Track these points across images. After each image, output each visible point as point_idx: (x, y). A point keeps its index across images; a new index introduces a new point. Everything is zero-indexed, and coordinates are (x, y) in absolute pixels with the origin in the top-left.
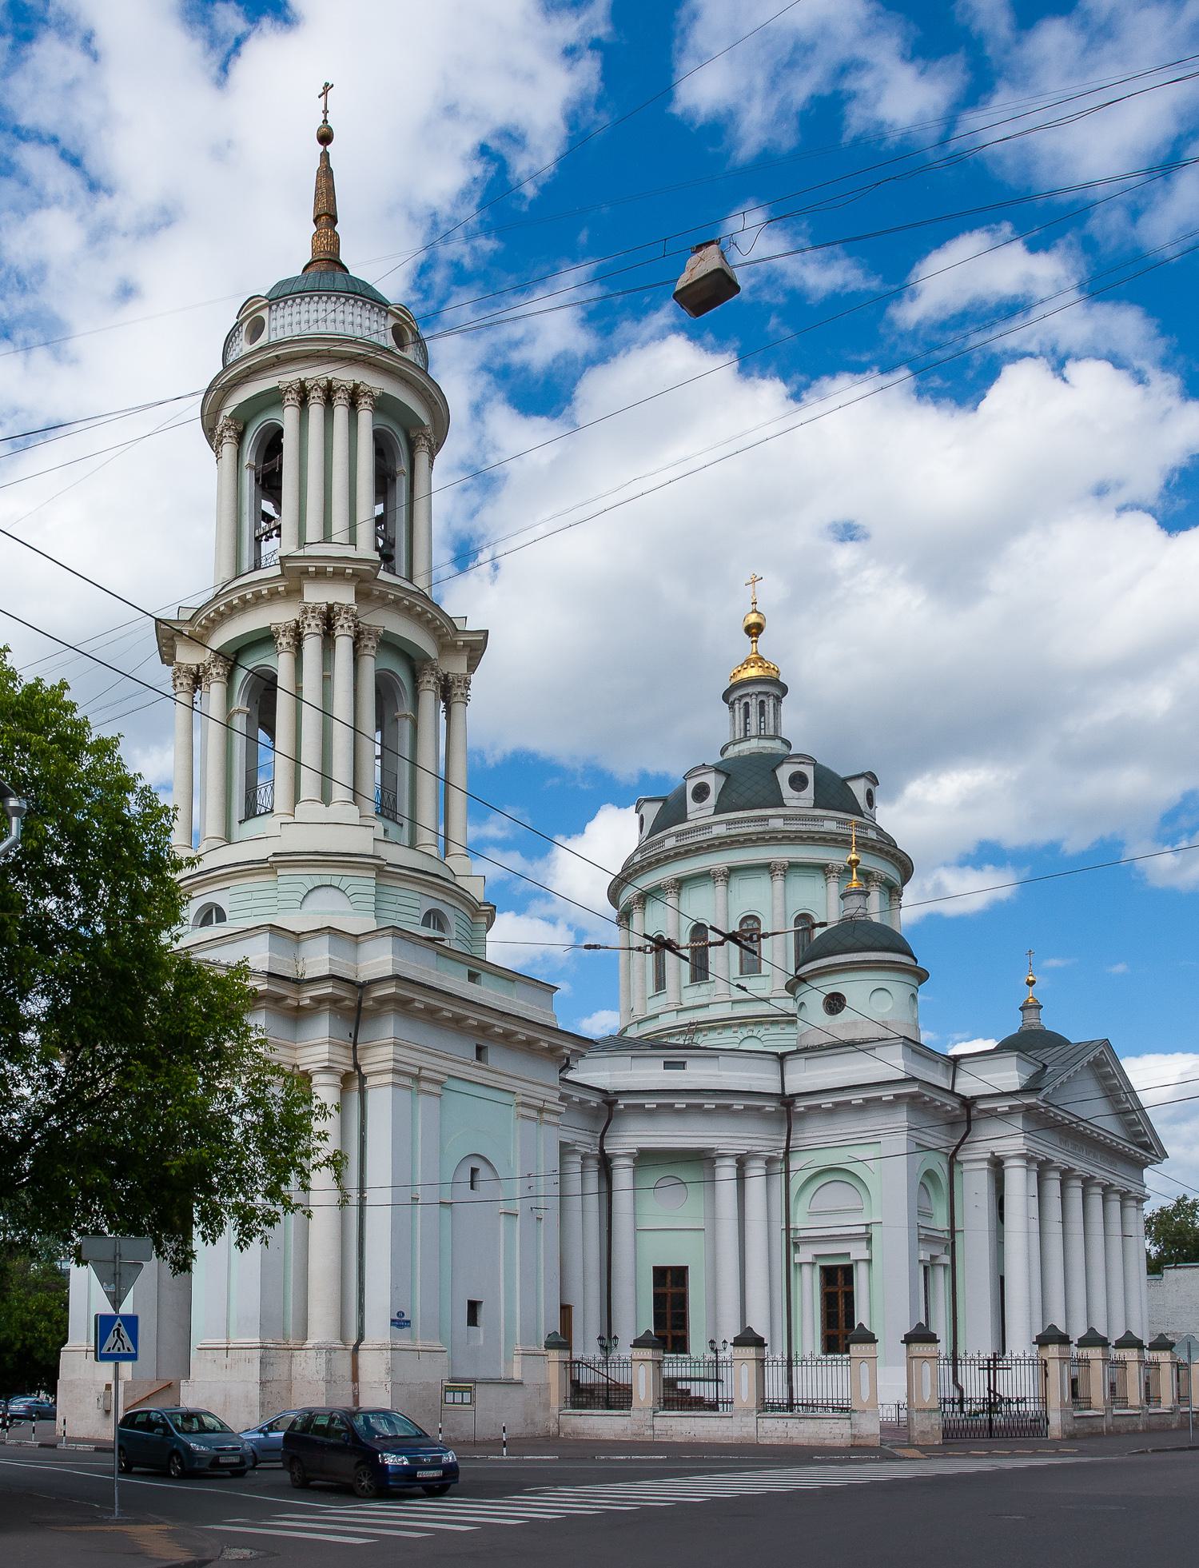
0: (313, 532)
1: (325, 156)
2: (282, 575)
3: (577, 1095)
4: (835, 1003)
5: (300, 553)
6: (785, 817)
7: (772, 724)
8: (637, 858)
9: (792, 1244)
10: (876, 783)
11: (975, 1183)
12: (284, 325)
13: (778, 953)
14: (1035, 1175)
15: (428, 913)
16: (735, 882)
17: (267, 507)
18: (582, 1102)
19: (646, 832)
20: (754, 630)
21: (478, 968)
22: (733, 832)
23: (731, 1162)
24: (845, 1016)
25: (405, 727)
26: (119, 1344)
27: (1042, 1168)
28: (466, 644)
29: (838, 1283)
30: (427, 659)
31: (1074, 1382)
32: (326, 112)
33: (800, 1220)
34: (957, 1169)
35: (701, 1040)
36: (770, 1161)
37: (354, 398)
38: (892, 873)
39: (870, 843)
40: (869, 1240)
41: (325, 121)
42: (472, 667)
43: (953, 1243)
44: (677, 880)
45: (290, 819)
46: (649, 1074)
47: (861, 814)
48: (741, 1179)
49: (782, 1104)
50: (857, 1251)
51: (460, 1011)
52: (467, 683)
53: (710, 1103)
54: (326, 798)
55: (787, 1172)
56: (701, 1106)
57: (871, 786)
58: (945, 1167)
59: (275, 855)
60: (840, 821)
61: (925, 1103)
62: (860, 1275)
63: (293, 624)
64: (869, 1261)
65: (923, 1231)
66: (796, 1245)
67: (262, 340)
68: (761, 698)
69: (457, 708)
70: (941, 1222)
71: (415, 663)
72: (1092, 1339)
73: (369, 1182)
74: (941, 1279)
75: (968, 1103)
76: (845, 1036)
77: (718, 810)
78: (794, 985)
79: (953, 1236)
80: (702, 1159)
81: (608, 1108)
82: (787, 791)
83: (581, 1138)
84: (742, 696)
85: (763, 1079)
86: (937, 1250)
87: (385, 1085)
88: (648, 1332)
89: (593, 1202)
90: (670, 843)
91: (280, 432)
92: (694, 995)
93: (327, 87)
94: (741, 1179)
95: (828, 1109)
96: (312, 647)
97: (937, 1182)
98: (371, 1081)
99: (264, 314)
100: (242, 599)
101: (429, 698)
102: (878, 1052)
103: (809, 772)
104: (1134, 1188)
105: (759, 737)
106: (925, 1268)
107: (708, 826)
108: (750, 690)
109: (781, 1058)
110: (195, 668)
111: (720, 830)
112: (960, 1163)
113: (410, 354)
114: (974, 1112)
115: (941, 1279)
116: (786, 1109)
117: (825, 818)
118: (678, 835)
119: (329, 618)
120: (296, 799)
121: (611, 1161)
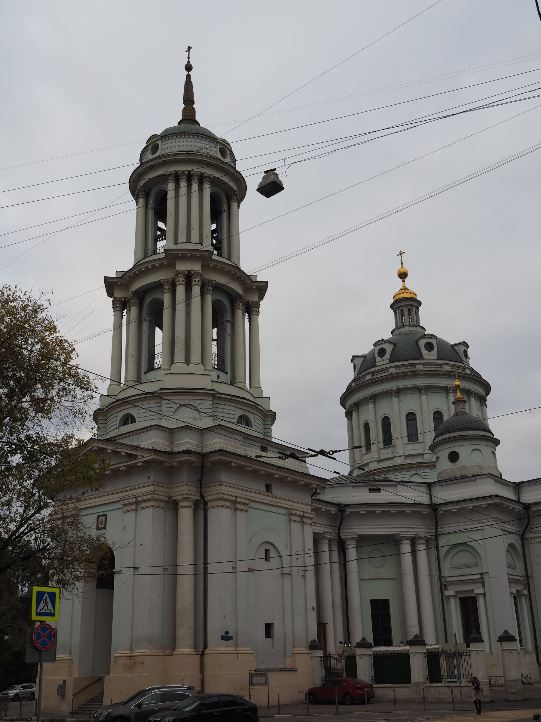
0: (182, 238)
1: (188, 76)
2: (166, 257)
3: (324, 508)
4: (454, 457)
5: (175, 247)
6: (424, 364)
8: (353, 385)
9: (443, 586)
12: (165, 148)
15: (240, 417)
16: (402, 396)
17: (161, 225)
18: (327, 511)
20: (403, 276)
21: (266, 444)
22: (399, 371)
25: (228, 327)
26: (46, 607)
28: (257, 288)
29: (469, 607)
30: (238, 294)
32: (189, 58)
33: (446, 572)
35: (392, 477)
37: (201, 179)
38: (480, 390)
39: (467, 376)
40: (483, 583)
41: (189, 62)
42: (261, 298)
43: (528, 583)
44: (373, 395)
45: (169, 372)
46: (363, 496)
47: (462, 362)
48: (414, 552)
50: (478, 590)
51: (256, 467)
52: (258, 306)
53: (394, 510)
54: (187, 362)
55: (438, 547)
56: (389, 512)
57: (465, 348)
58: (519, 541)
59: (161, 389)
60: (451, 366)
61: (504, 508)
62: (481, 602)
63: (171, 279)
64: (484, 594)
65: (511, 577)
66: (446, 586)
67: (158, 154)
68: (409, 307)
69: (254, 317)
70: (520, 570)
71: (233, 298)
73: (210, 560)
75: (527, 507)
76: (458, 474)
77: (391, 361)
78: (432, 448)
79: (528, 580)
80: (393, 541)
81: (341, 513)
82: (424, 352)
83: (327, 530)
84: (408, 305)
85: (421, 497)
86: (520, 587)
88: (314, 640)
89: (336, 567)
90: (369, 377)
91: (166, 193)
92: (386, 453)
93: (189, 48)
94: (414, 552)
95: (485, 508)
96: (180, 290)
97: (521, 551)
98: (210, 504)
99: (159, 143)
100: (134, 274)
101: (239, 313)
103: (433, 342)
105: (409, 326)
106: (515, 598)
107: (387, 369)
109: (429, 486)
110: (123, 299)
111: (393, 370)
112: (527, 539)
113: (227, 160)
114: (530, 512)
116: (434, 512)
117: (444, 364)
118: (373, 373)
119: (189, 277)
120: (172, 362)
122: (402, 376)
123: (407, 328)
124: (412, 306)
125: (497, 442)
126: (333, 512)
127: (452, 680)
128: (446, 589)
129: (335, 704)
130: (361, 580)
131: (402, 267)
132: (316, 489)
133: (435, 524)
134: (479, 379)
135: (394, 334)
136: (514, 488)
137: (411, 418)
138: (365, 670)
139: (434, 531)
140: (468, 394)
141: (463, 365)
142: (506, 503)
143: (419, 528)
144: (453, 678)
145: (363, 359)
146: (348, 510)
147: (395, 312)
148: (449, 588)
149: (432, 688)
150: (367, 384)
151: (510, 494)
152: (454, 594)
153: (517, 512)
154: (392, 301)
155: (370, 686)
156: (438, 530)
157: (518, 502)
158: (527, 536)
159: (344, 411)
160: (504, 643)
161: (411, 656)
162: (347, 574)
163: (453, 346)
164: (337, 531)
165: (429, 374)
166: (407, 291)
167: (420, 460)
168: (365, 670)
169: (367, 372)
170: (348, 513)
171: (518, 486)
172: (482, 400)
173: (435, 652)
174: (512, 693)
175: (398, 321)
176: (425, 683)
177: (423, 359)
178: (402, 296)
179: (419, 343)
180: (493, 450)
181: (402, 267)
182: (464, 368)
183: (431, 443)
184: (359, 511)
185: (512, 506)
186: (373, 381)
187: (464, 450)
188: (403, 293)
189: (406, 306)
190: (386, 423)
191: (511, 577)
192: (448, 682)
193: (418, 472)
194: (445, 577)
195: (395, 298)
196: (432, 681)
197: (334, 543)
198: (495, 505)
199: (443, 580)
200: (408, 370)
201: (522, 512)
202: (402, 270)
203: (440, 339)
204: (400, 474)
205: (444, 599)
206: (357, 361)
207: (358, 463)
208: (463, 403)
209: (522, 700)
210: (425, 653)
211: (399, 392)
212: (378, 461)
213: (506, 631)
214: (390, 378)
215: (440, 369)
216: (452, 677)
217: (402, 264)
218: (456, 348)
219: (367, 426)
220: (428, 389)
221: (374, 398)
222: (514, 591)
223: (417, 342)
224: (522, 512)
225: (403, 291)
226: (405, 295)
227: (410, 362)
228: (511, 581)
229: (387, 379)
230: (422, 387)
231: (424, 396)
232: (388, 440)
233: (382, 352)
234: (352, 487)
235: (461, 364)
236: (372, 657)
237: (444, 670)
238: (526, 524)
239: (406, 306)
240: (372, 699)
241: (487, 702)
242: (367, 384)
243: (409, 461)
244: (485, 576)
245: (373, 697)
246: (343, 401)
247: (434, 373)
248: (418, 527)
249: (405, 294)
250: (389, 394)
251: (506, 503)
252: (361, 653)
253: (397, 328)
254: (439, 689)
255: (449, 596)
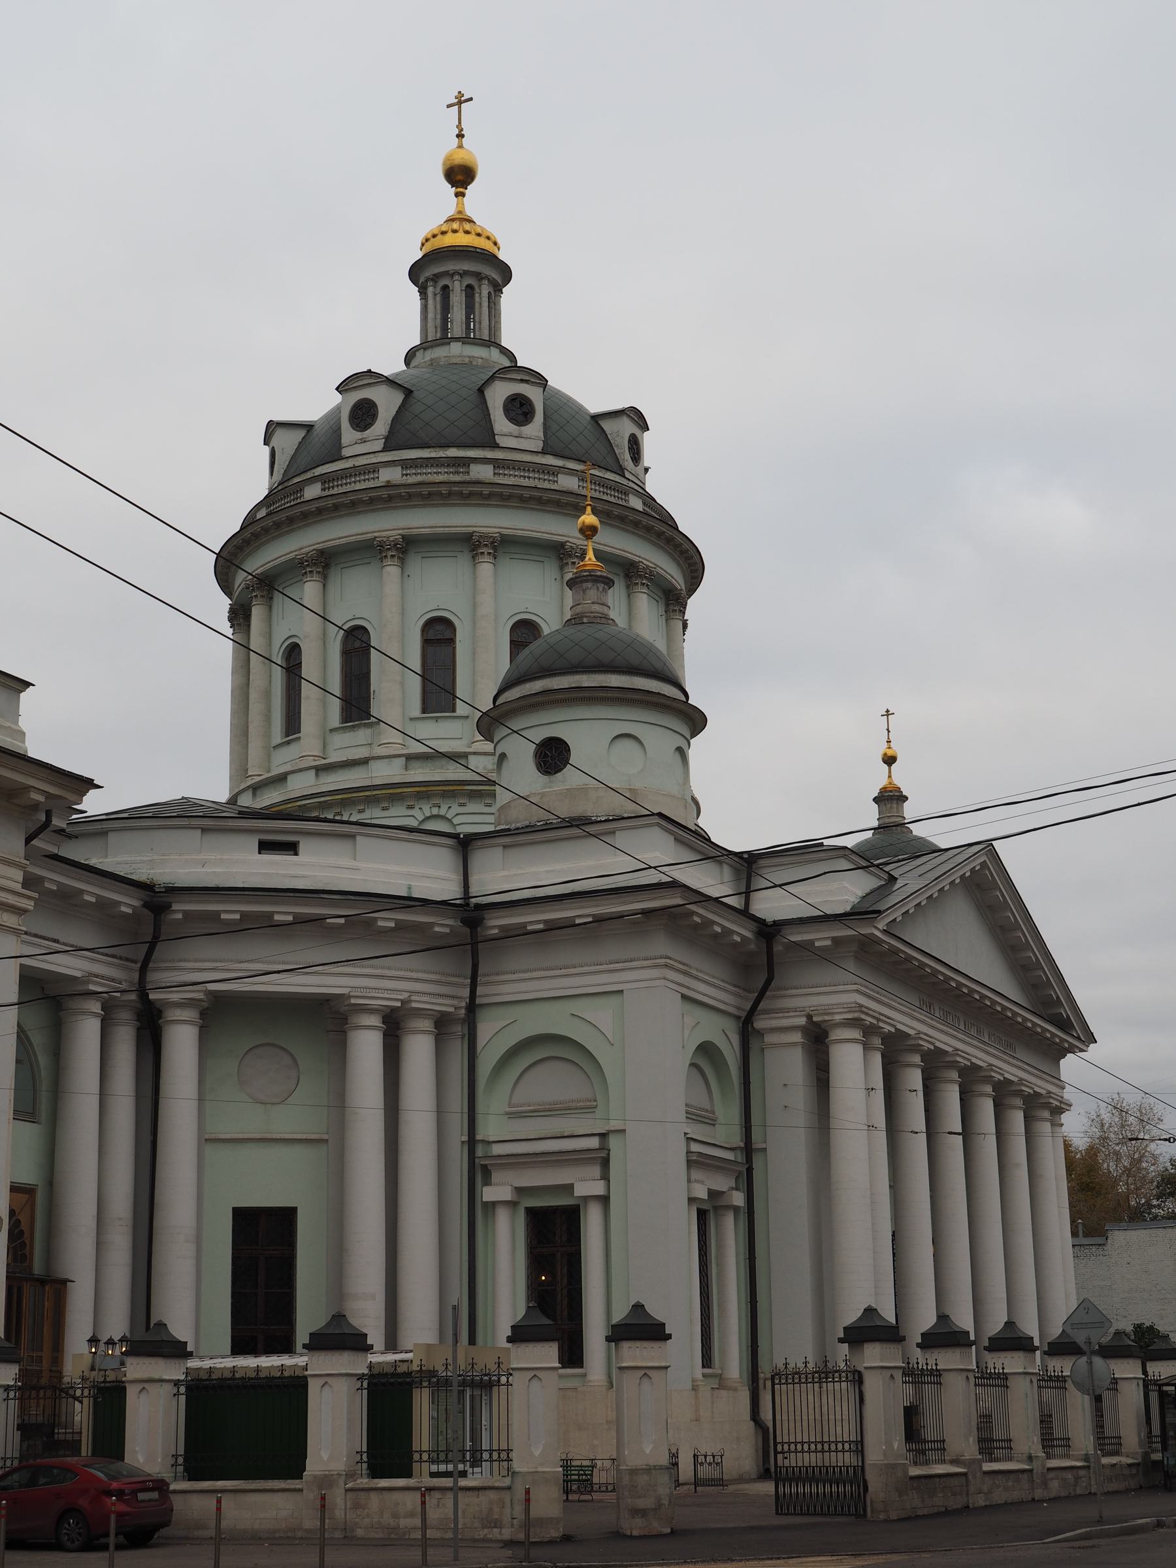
3: (92, 891)
4: (552, 756)
6: (497, 464)
7: (485, 323)
9: (479, 1171)
10: (645, 427)
11: (786, 1066)
13: (482, 669)
14: (877, 1059)
16: (416, 564)
18: (103, 905)
19: (278, 477)
20: (460, 176)
22: (411, 480)
23: (375, 1020)
24: (569, 778)
27: (893, 1050)
29: (554, 1236)
31: (911, 1413)
33: (492, 1127)
34: (754, 1045)
36: (442, 1023)
40: (605, 1163)
43: (750, 1171)
44: (322, 552)
46: (241, 863)
47: (621, 471)
49: (465, 921)
50: (587, 1185)
57: (637, 432)
58: (735, 1039)
64: (605, 1200)
65: (695, 1147)
66: (487, 1172)
70: (728, 1132)
72: (945, 1336)
74: (729, 1233)
75: (769, 931)
76: (565, 810)
79: (749, 1159)
80: (328, 1018)
82: (501, 424)
85: (428, 875)
86: (722, 1183)
87: (794, 1044)
90: (312, 492)
97: (732, 1067)
102: (621, 839)
104: (1042, 1086)
105: (465, 340)
106: (702, 1215)
107: (374, 469)
108: (451, 266)
112: (760, 1034)
114: (778, 948)
115: (729, 1233)
116: (470, 932)
118: (326, 479)
121: (160, 1014)
122: (420, 495)
123: (456, 348)
124: (479, 276)
125: (696, 721)
126: (124, 909)
127: (442, 1468)
128: (487, 1182)
129: (105, 1548)
130: (207, 1140)
131: (460, 146)
132: (49, 814)
133: (469, 972)
134: (669, 532)
135: (413, 364)
136: (737, 871)
137: (439, 635)
138: (152, 1432)
139: (466, 993)
140: (628, 576)
141: (625, 482)
142: (701, 911)
143: (417, 980)
144: (447, 1462)
145: (300, 434)
146: (180, 907)
147: (423, 292)
148: (496, 1176)
149: (373, 1495)
150: (305, 516)
151: (712, 882)
152: (508, 1198)
153: (735, 944)
154: (419, 255)
155: (160, 1486)
156: (480, 990)
157: (745, 913)
158: (760, 1023)
159: (225, 603)
160: (625, 1345)
161: (313, 1387)
162: (436, 1241)
163: (596, 418)
164: (136, 976)
165: (510, 497)
166: (467, 226)
167: (453, 772)
168: (152, 1432)
169: (309, 475)
170: (180, 916)
171: (748, 865)
172: (674, 602)
173: (395, 1375)
174: (636, 1512)
175: (430, 324)
176: (350, 1475)
177: (495, 446)
178: (450, 240)
179: (489, 393)
180: (682, 743)
181: (460, 146)
182: (625, 492)
183: (486, 704)
184: (218, 913)
185: (722, 922)
186: (322, 504)
187: (588, 735)
188: (455, 231)
189: (460, 276)
190: (357, 645)
191: (695, 1147)
192: (433, 1475)
193: (443, 812)
194: (489, 1143)
195: (428, 247)
196: (376, 1471)
197: (125, 1015)
198: (667, 914)
199: (480, 1151)
200: (440, 478)
201: (752, 946)
202: (460, 158)
203: (558, 394)
204: (386, 814)
205: (477, 1213)
206: (279, 437)
207: (257, 772)
208: (601, 586)
209: (666, 1535)
210: (361, 1377)
211: (406, 548)
212: (319, 770)
213: (638, 1307)
214: (379, 499)
215: (546, 485)
216: (442, 1456)
217: (460, 136)
218: (607, 425)
219: (293, 652)
220: (503, 546)
221: (324, 562)
222: (701, 1193)
223: (481, 391)
224: (752, 946)
225: (455, 226)
226: (461, 240)
227: (453, 452)
228: (694, 1162)
229: (372, 501)
230: (484, 536)
231: (486, 568)
232: (356, 705)
233: (363, 414)
234: (204, 830)
235: (618, 478)
236: (183, 1389)
237: (423, 1437)
238: (760, 985)
239: (460, 276)
240: (164, 1532)
241: (551, 1542)
242: (305, 516)
243: (420, 773)
244: (614, 1142)
245: (166, 1524)
246: (227, 563)
247: (526, 494)
248: (414, 975)
249: (461, 234)
250: (372, 550)
251: (701, 911)
252: (146, 1376)
253: (425, 345)
254: (396, 1496)
255: (494, 1204)
